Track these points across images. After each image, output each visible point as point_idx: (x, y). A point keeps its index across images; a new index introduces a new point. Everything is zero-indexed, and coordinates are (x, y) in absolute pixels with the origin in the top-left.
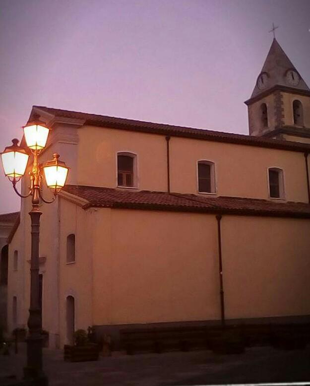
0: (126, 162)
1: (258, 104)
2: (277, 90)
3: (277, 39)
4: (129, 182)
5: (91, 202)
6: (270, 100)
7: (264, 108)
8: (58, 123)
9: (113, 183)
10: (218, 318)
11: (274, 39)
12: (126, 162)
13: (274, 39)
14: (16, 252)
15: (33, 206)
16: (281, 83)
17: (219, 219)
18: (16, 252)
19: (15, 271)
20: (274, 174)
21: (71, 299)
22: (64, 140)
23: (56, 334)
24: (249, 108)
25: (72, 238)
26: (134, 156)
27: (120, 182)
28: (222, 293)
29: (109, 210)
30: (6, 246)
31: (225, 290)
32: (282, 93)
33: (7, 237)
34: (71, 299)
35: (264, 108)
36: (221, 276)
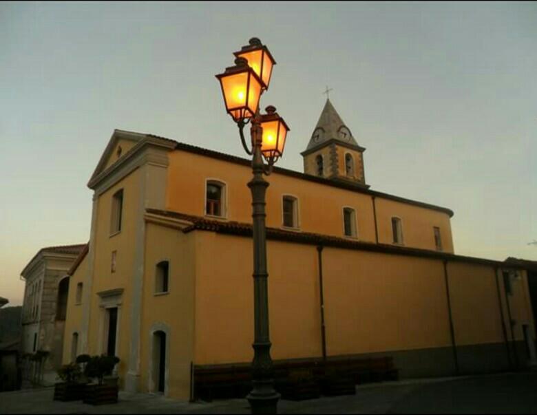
0: (214, 194)
1: (313, 157)
2: (332, 143)
3: (330, 100)
4: (217, 211)
5: (196, 223)
6: (325, 153)
7: (320, 159)
8: (150, 144)
9: (202, 213)
10: (320, 355)
11: (328, 100)
12: (214, 194)
13: (328, 100)
14: (80, 285)
15: (147, 222)
16: (335, 136)
17: (320, 250)
18: (80, 285)
19: (78, 305)
20: (347, 212)
21: (161, 336)
22: (154, 162)
23: (137, 376)
24: (304, 160)
25: (164, 267)
26: (222, 185)
27: (208, 212)
28: (323, 328)
29: (213, 234)
30: (65, 278)
31: (326, 325)
32: (337, 146)
33: (68, 269)
34: (161, 336)
35: (320, 159)
36: (322, 310)
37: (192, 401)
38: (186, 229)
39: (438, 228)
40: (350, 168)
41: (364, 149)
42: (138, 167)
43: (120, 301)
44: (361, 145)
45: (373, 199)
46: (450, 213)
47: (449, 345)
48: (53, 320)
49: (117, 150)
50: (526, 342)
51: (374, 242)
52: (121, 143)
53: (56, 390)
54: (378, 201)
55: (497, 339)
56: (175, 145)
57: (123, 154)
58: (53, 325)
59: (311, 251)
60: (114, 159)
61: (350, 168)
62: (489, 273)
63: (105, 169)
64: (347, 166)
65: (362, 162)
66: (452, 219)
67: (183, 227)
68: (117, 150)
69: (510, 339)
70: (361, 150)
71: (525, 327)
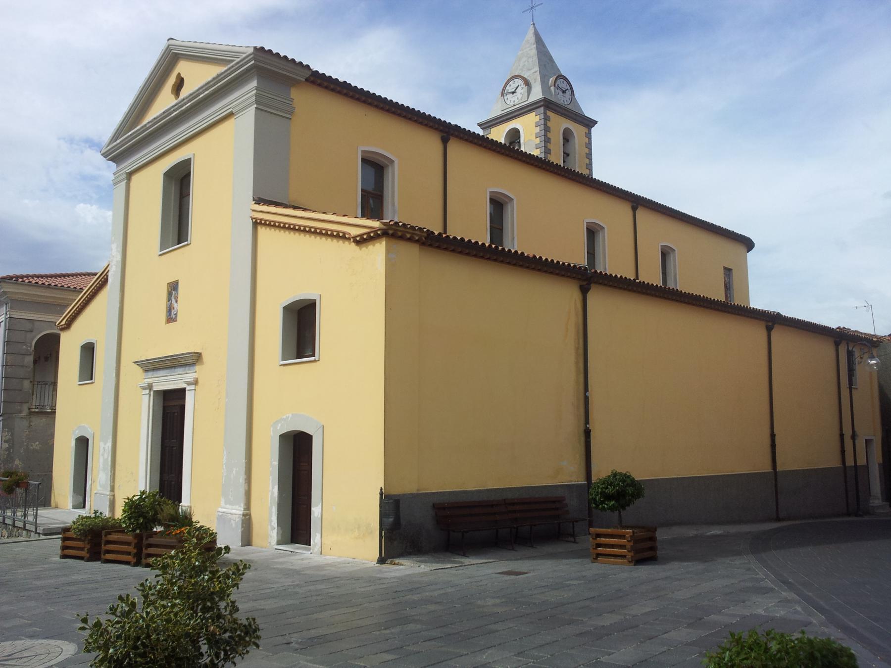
10: (578, 479)
17: (584, 291)
18: (88, 350)
28: (587, 433)
37: (382, 561)
38: (361, 235)
39: (730, 270)
40: (568, 155)
41: (595, 122)
42: (231, 115)
43: (190, 376)
44: (588, 113)
45: (634, 209)
46: (748, 244)
47: (582, 481)
48: (25, 413)
49: (172, 80)
50: (867, 467)
51: (660, 284)
52: (183, 68)
53: (64, 539)
54: (641, 213)
55: (832, 461)
56: (307, 74)
57: (185, 92)
58: (25, 423)
59: (562, 297)
60: (165, 101)
61: (568, 155)
62: (826, 350)
63: (145, 122)
64: (564, 153)
65: (589, 145)
66: (750, 255)
67: (354, 232)
68: (172, 80)
69: (850, 462)
70: (589, 123)
71: (868, 442)
